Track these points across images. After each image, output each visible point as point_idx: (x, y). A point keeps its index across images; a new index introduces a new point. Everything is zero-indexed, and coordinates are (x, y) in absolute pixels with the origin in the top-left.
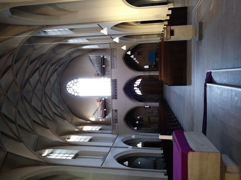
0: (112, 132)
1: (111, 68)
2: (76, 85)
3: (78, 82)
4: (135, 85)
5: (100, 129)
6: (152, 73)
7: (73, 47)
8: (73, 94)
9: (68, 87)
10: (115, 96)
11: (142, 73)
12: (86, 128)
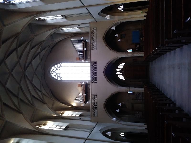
0: (91, 119)
1: (91, 49)
2: (59, 70)
3: (61, 66)
4: (118, 70)
5: (81, 115)
6: (136, 55)
7: (54, 28)
8: (56, 78)
9: (51, 72)
10: (94, 79)
11: (124, 54)
12: (67, 114)
